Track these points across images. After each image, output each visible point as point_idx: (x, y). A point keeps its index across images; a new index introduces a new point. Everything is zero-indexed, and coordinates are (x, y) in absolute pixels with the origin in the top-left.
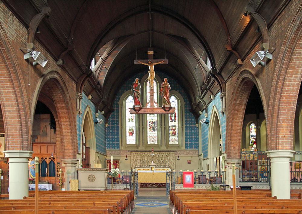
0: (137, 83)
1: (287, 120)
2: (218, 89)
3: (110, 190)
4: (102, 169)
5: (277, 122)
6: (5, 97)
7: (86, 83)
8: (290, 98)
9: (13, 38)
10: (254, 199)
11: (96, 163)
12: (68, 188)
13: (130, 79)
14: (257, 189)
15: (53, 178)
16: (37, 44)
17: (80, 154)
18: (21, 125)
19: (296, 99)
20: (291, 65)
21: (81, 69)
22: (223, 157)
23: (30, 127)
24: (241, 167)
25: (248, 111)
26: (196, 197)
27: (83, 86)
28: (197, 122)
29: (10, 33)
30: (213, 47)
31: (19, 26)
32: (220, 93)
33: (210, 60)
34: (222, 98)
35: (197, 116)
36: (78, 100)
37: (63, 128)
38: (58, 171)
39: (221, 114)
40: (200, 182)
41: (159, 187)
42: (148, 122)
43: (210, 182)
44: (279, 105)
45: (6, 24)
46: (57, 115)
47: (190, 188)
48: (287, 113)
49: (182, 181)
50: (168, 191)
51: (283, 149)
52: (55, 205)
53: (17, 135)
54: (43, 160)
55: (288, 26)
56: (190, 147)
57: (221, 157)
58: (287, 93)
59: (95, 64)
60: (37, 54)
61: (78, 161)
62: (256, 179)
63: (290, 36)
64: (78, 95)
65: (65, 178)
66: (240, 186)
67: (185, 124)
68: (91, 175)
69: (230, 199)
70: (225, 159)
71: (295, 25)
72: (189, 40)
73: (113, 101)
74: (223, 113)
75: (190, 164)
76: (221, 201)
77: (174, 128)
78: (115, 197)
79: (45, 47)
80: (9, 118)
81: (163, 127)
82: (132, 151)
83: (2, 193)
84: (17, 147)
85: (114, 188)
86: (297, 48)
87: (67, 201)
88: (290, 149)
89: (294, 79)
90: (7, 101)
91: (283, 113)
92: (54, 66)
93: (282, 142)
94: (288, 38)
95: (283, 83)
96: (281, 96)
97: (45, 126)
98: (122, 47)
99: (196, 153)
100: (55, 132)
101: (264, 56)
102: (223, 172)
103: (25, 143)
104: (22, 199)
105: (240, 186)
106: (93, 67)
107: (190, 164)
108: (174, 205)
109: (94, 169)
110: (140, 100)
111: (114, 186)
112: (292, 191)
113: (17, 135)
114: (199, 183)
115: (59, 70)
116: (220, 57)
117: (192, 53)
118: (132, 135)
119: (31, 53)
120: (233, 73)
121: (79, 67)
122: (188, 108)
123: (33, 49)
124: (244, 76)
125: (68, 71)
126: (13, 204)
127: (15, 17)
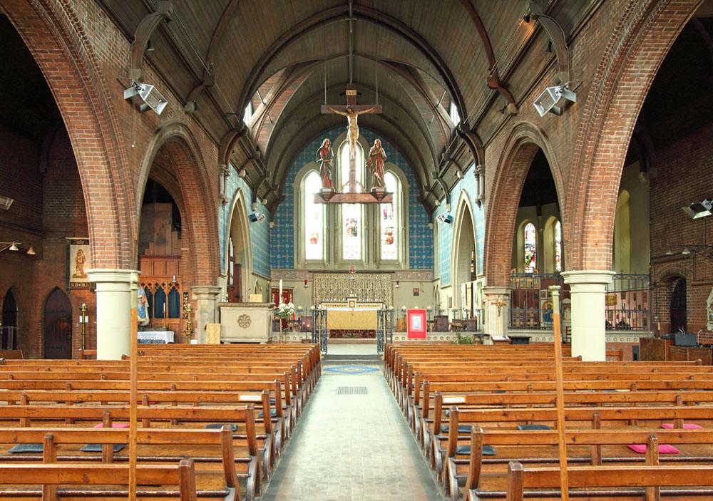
0: (326, 147)
1: (602, 215)
2: (470, 160)
3: (277, 342)
4: (262, 304)
5: (584, 218)
6: (88, 168)
7: (236, 148)
8: (608, 174)
9: (104, 58)
10: (542, 362)
11: (252, 293)
12: (202, 340)
13: (313, 143)
14: (539, 343)
15: (176, 321)
16: (149, 72)
17: (224, 277)
18: (118, 222)
19: (618, 175)
20: (612, 111)
21: (227, 121)
22: (479, 284)
23: (134, 226)
24: (508, 303)
25: (524, 201)
26: (435, 356)
27: (231, 152)
28: (431, 219)
29: (99, 48)
30: (463, 83)
31: (116, 37)
32: (474, 166)
33: (457, 104)
34: (477, 176)
35: (431, 210)
36: (222, 178)
37: (194, 228)
38: (184, 308)
39: (475, 206)
40: (437, 328)
41: (363, 337)
42: (344, 220)
43: (455, 328)
44: (588, 187)
45: (93, 31)
46: (183, 206)
47: (419, 340)
48: (602, 202)
49: (405, 328)
50: (380, 344)
51: (594, 269)
52: (179, 373)
53: (111, 240)
54: (157, 288)
55: (608, 37)
56: (419, 265)
57: (475, 283)
58: (602, 165)
59: (253, 112)
60: (148, 88)
61: (220, 289)
62: (536, 323)
63: (612, 56)
64: (222, 169)
65: (196, 322)
66: (510, 337)
67: (410, 224)
68: (244, 315)
69: (496, 360)
70: (483, 287)
71: (622, 37)
72: (418, 70)
73: (283, 181)
74: (479, 203)
75: (418, 295)
76: (482, 364)
77: (390, 231)
78: (288, 356)
79: (163, 78)
80: (97, 209)
81: (371, 226)
82: (315, 272)
83: (87, 347)
84: (111, 262)
85: (284, 340)
86: (623, 80)
87: (200, 364)
88: (607, 269)
89: (616, 139)
90: (92, 177)
91: (595, 201)
92: (179, 114)
93: (592, 255)
94: (607, 61)
95: (597, 146)
96: (592, 169)
97: (163, 225)
98: (300, 82)
99: (429, 276)
100: (179, 237)
101: (560, 95)
102: (478, 311)
103: (125, 254)
104: (120, 359)
105: (510, 337)
106: (249, 119)
107: (418, 295)
108: (393, 370)
109: (249, 305)
110: (330, 176)
111: (284, 336)
112: (608, 345)
113: (111, 240)
114: (436, 330)
115: (188, 121)
116: (475, 100)
117: (425, 95)
118: (316, 243)
119: (137, 87)
120: (500, 129)
121: (223, 116)
122: (415, 195)
123: (141, 81)
124: (520, 134)
125: (204, 124)
126: (102, 369)
127: (108, 19)
